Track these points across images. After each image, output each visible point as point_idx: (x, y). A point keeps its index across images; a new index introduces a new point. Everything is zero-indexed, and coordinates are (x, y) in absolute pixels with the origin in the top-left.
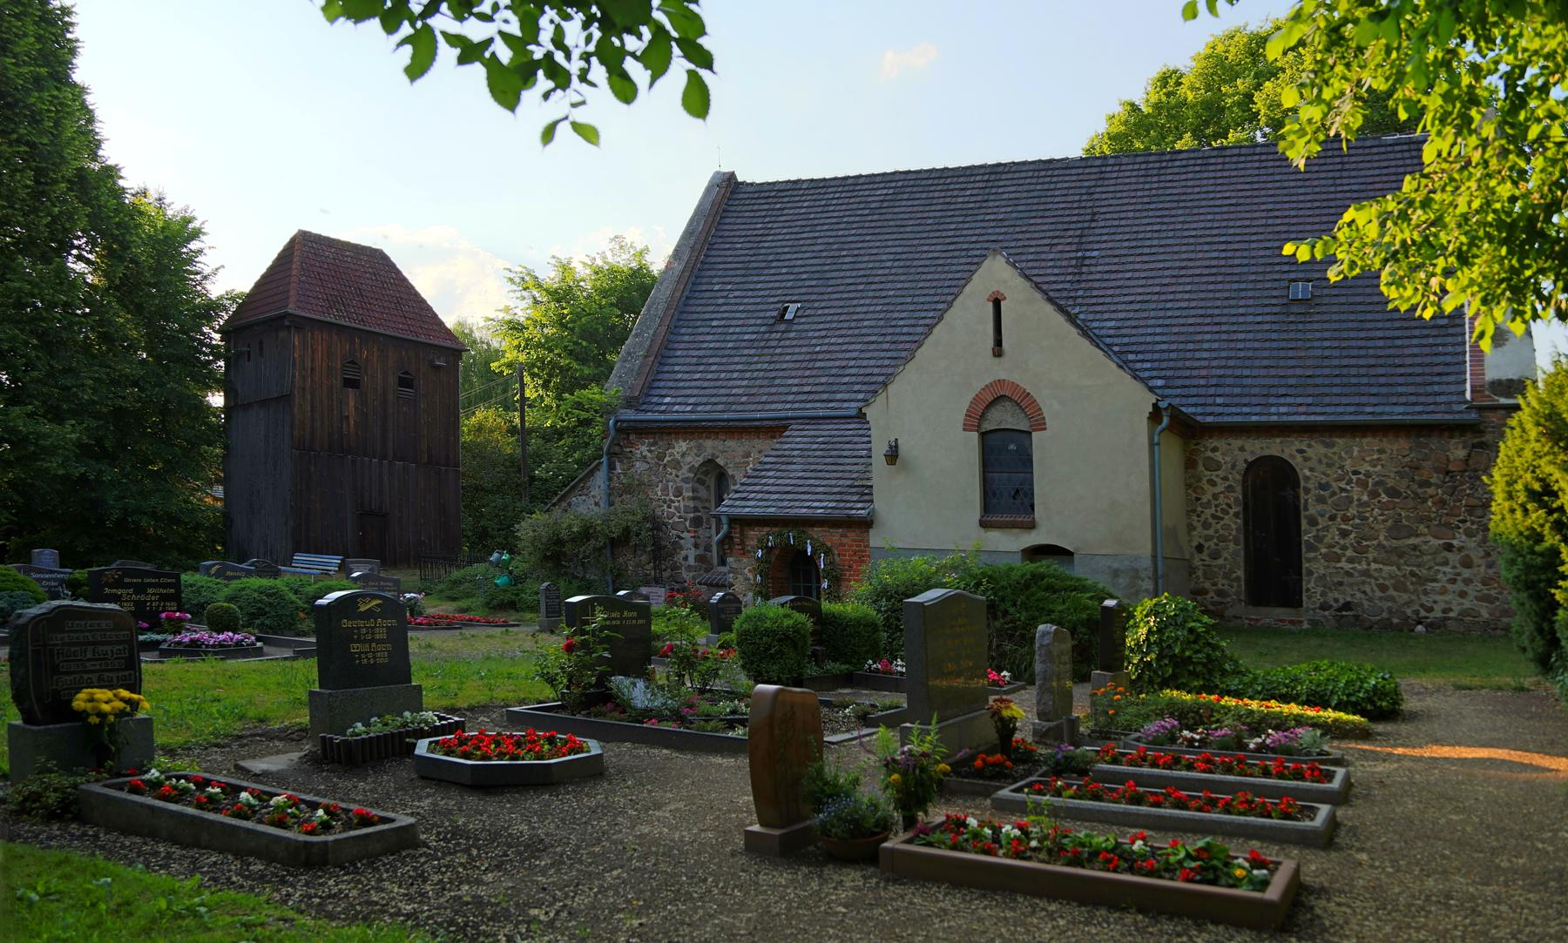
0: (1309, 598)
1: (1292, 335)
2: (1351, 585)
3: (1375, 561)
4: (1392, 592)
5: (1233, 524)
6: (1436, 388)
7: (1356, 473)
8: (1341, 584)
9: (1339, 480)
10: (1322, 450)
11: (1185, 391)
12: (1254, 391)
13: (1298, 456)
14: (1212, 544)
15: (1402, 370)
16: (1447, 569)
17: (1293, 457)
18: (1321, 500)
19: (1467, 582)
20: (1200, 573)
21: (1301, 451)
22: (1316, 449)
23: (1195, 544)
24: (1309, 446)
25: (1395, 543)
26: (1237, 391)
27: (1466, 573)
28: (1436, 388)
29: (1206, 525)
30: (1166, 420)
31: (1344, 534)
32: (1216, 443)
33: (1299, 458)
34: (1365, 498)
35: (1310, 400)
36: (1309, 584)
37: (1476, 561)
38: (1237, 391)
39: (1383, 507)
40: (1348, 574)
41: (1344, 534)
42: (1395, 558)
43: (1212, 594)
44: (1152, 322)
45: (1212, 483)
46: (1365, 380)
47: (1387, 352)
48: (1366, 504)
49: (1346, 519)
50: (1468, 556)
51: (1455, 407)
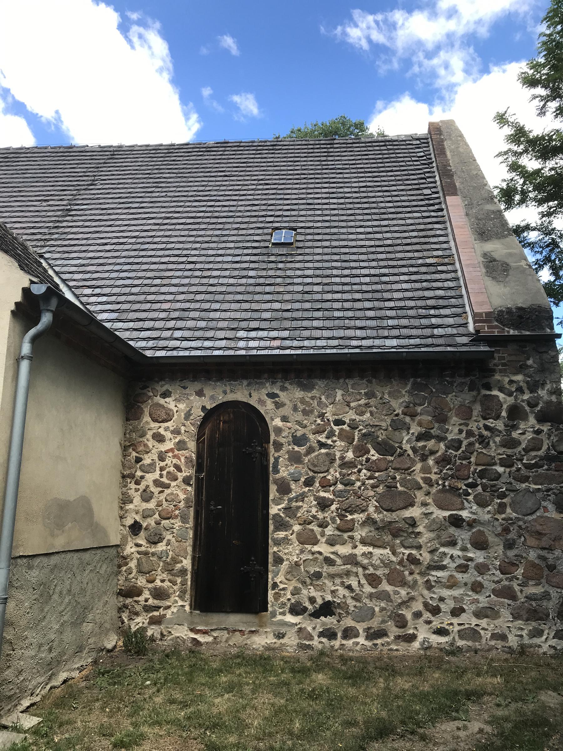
0: (277, 596)
1: (271, 273)
2: (332, 576)
3: (364, 542)
4: (386, 586)
5: (182, 493)
6: (434, 321)
7: (338, 422)
8: (318, 575)
9: (318, 432)
10: (299, 394)
11: (139, 325)
12: (221, 324)
13: (269, 402)
14: (151, 521)
15: (392, 304)
16: (456, 552)
17: (261, 401)
18: (295, 458)
19: (482, 569)
20: (133, 564)
21: (272, 396)
22: (291, 395)
23: (129, 521)
24: (283, 389)
25: (389, 517)
26: (202, 324)
27: (479, 556)
28: (434, 321)
29: (147, 497)
30: (46, 319)
31: (323, 505)
32: (167, 387)
33: (269, 403)
34: (350, 455)
35: (286, 334)
36: (278, 576)
37: (491, 539)
38: (202, 324)
39: (372, 467)
40: (329, 561)
41: (323, 505)
42: (388, 538)
43: (146, 594)
44: (122, 260)
45: (160, 438)
46: (350, 314)
47: (375, 287)
48: (350, 465)
49: (325, 485)
50: (481, 533)
51: (460, 340)
